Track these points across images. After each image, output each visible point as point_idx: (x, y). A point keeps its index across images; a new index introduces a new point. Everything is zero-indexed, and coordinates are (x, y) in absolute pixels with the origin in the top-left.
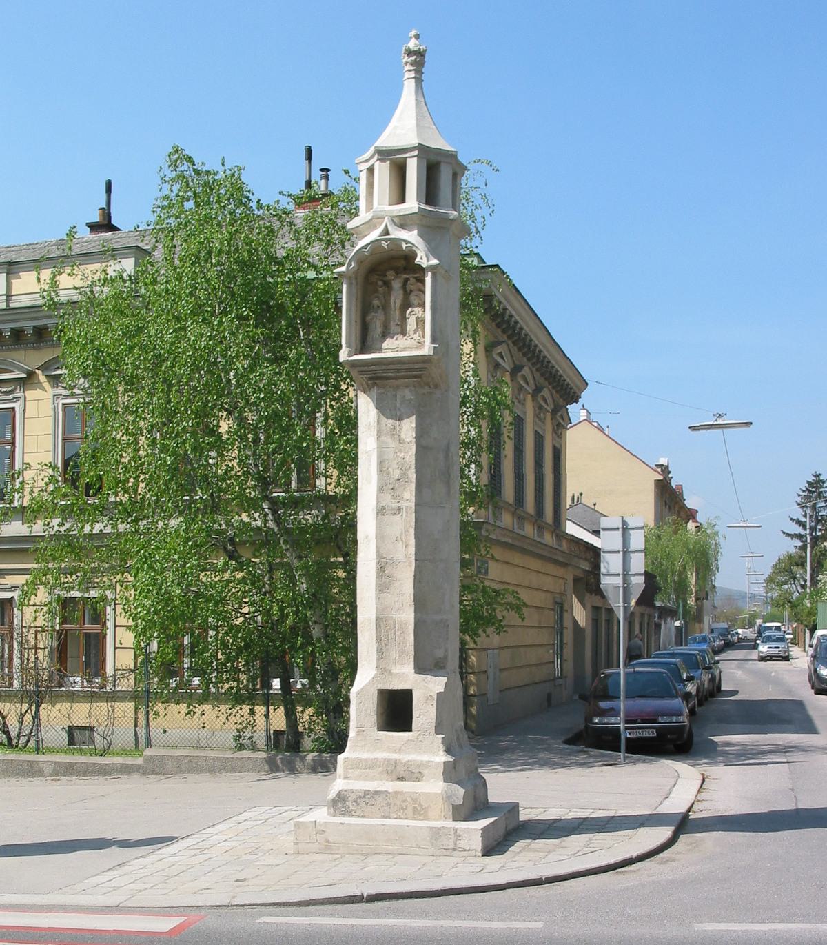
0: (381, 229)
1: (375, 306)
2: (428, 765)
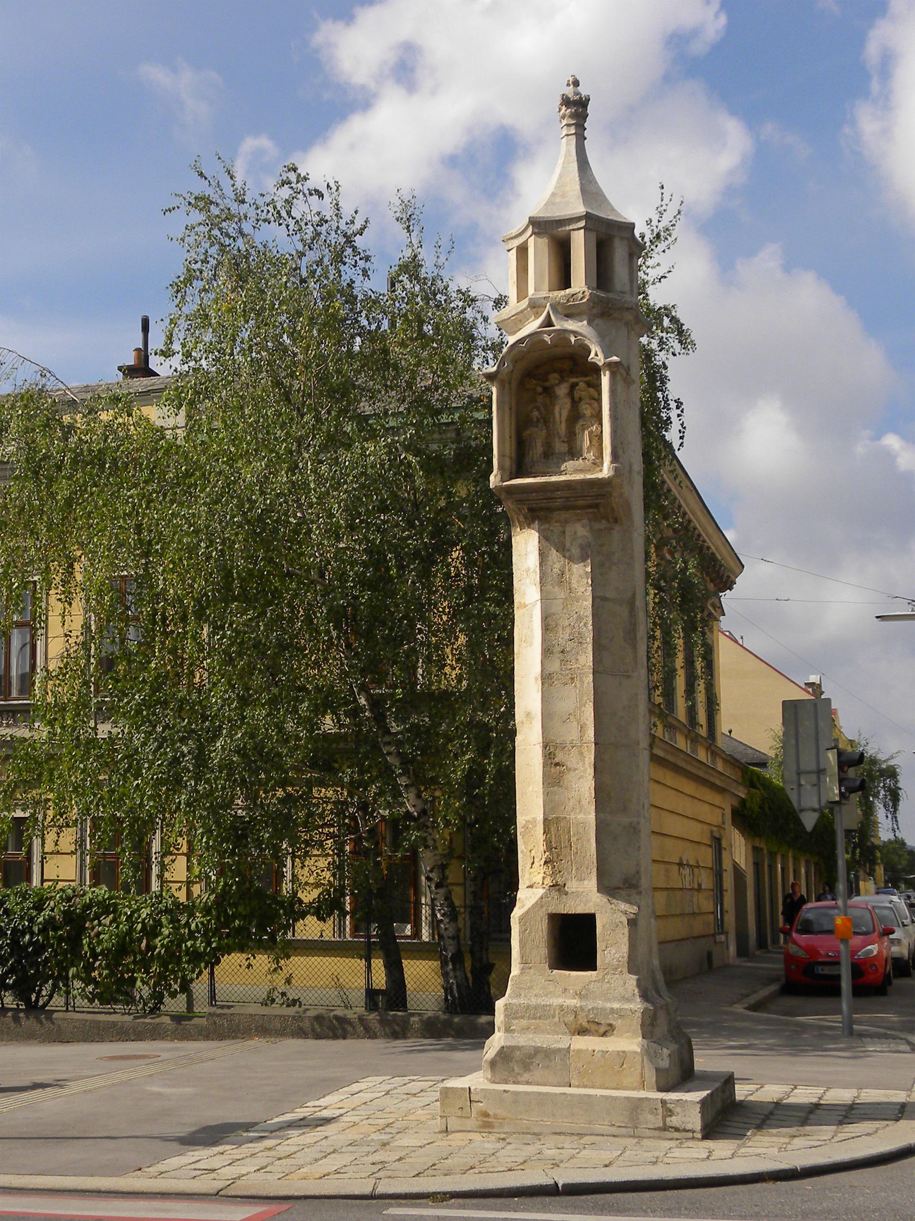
1: (535, 419)
2: (620, 1014)
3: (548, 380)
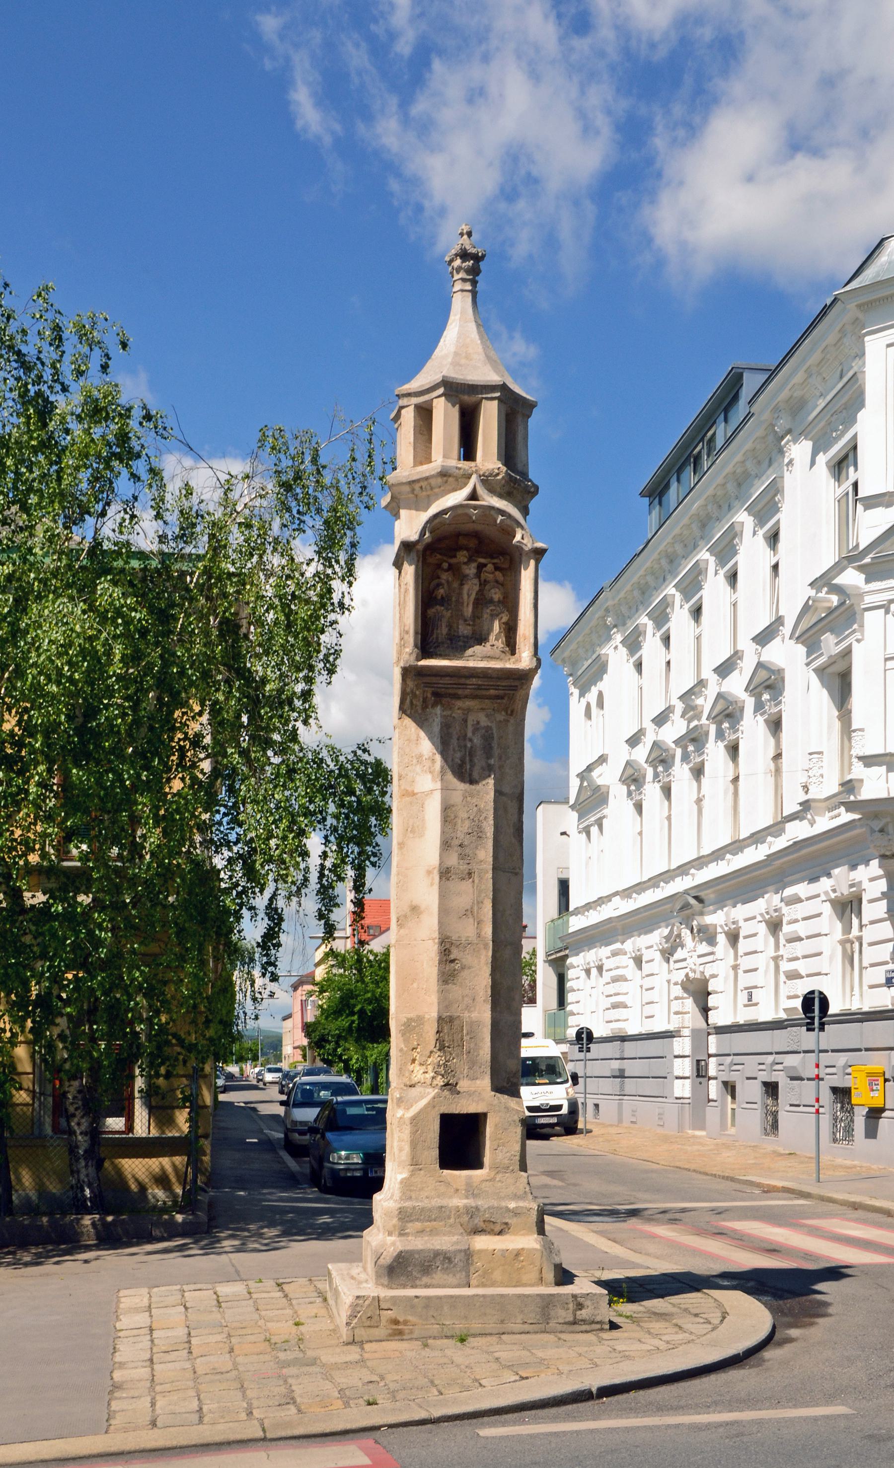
0: (466, 491)
2: (516, 1213)
3: (455, 556)
